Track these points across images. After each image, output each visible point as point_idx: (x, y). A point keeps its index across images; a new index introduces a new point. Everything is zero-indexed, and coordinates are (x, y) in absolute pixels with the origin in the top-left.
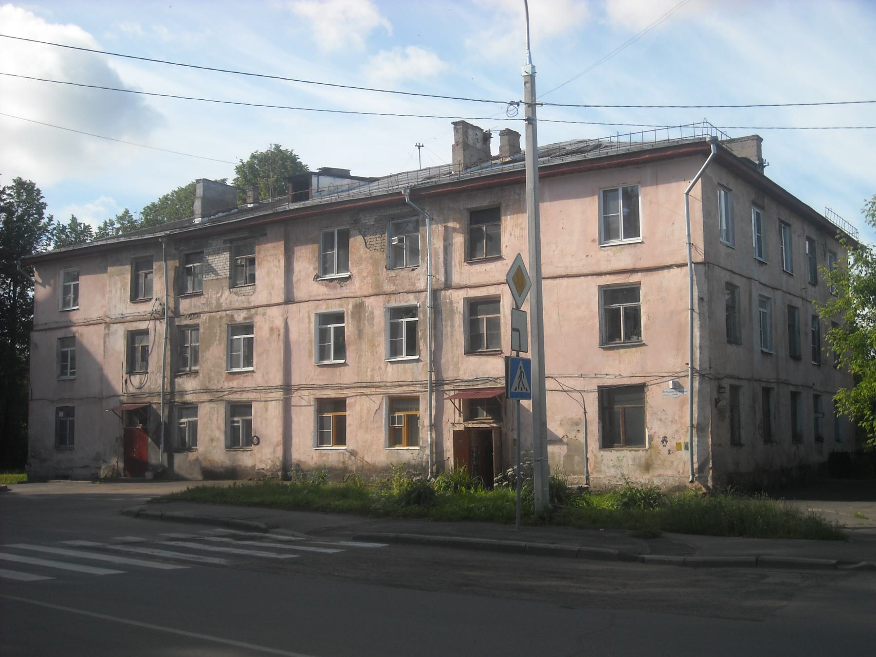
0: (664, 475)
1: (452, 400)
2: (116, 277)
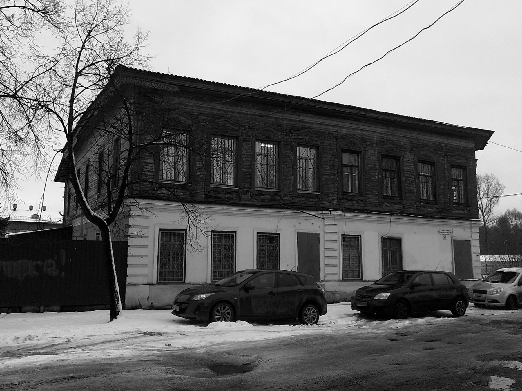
1: (493, 293)
2: (495, 224)
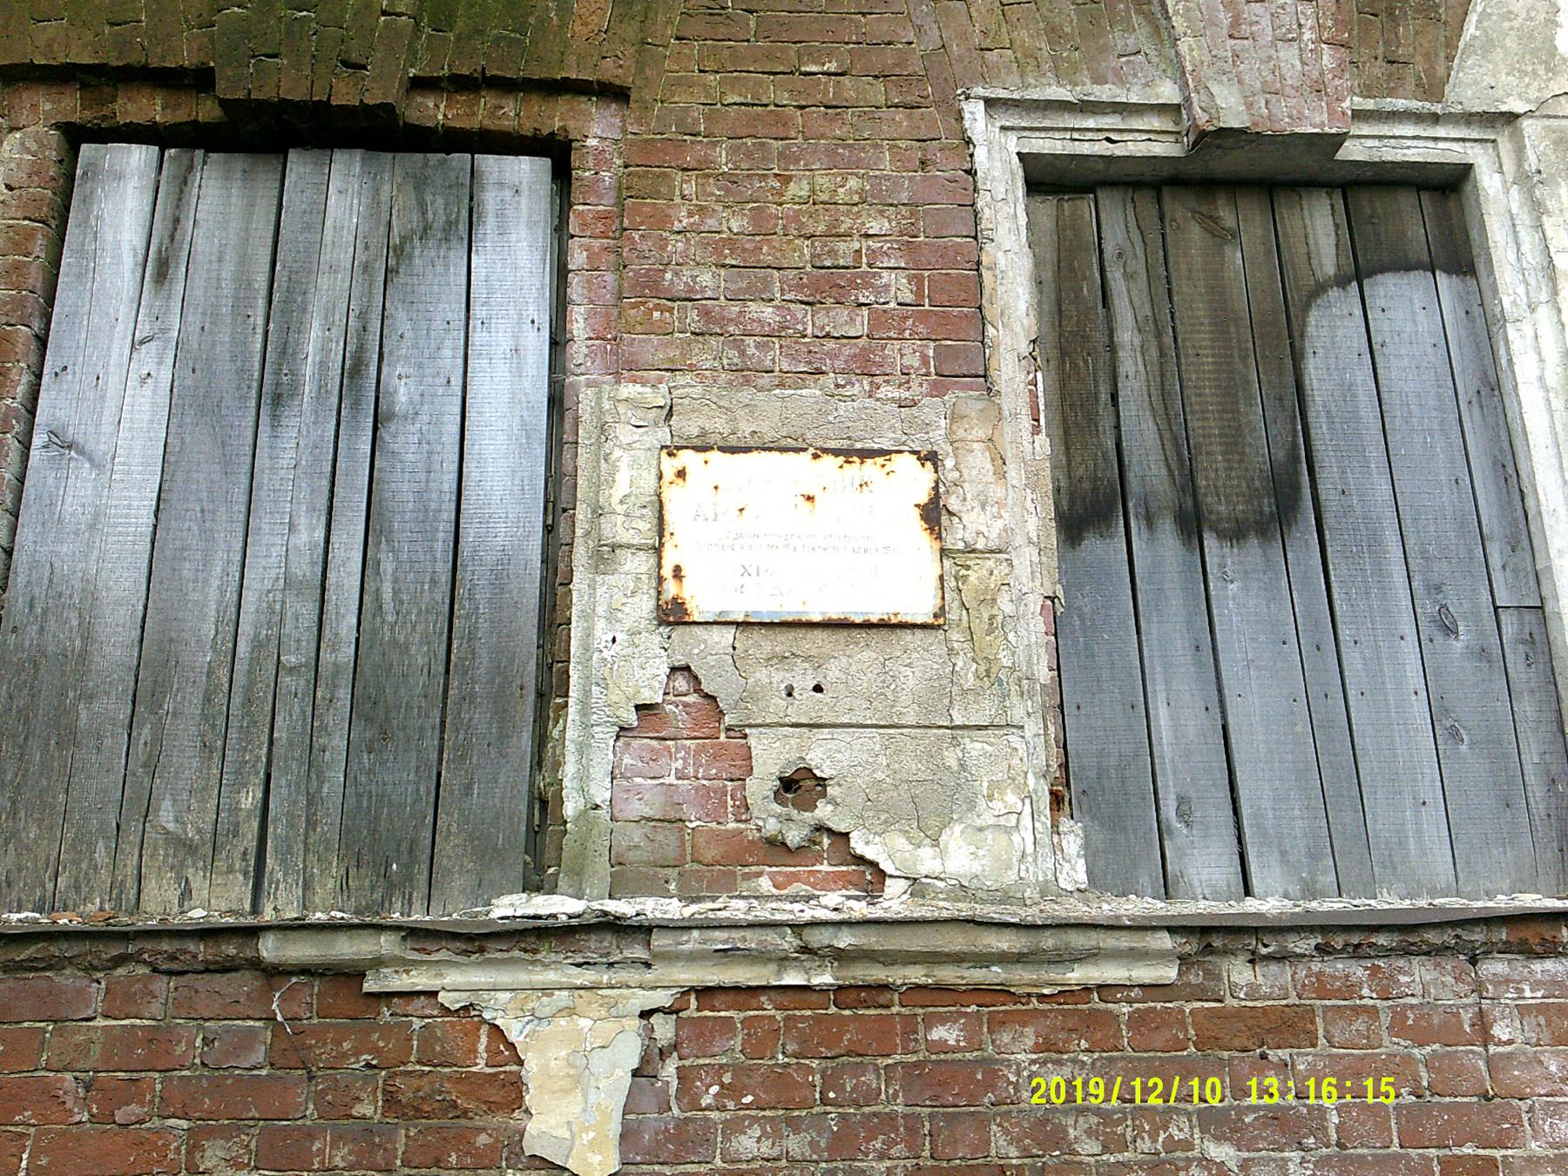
0: (207, 690)
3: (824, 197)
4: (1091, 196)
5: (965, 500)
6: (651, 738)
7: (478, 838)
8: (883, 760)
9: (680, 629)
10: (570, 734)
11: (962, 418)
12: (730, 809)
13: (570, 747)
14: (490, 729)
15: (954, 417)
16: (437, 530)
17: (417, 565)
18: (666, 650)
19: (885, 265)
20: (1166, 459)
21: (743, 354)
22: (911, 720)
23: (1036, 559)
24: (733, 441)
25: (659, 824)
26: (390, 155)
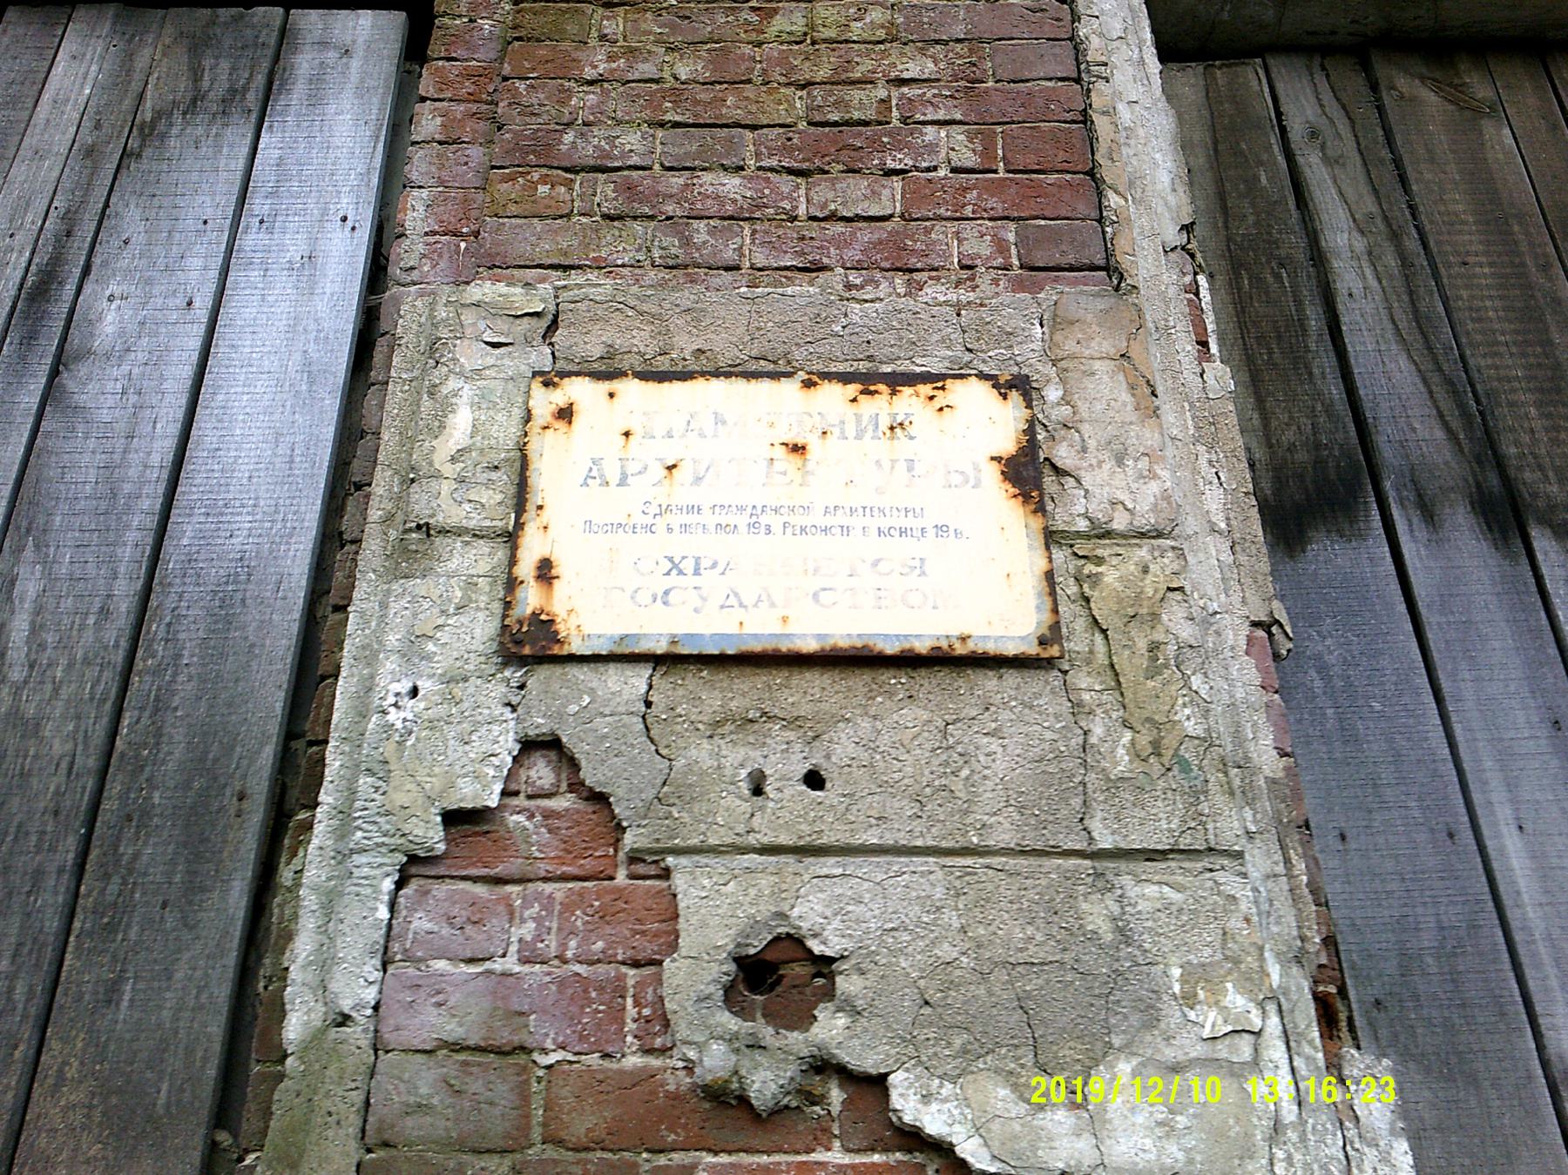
3: (831, 33)
4: (1258, 61)
5: (1084, 450)
6: (475, 880)
7: (119, 1091)
8: (952, 918)
9: (543, 672)
10: (312, 874)
11: (1072, 323)
12: (630, 1026)
13: (309, 900)
14: (169, 875)
15: (1056, 322)
16: (127, 526)
17: (81, 584)
18: (514, 709)
19: (929, 118)
20: (1441, 415)
21: (687, 242)
22: (1004, 836)
23: (1227, 557)
24: (663, 364)
25: (478, 1058)
26: (161, 12)
